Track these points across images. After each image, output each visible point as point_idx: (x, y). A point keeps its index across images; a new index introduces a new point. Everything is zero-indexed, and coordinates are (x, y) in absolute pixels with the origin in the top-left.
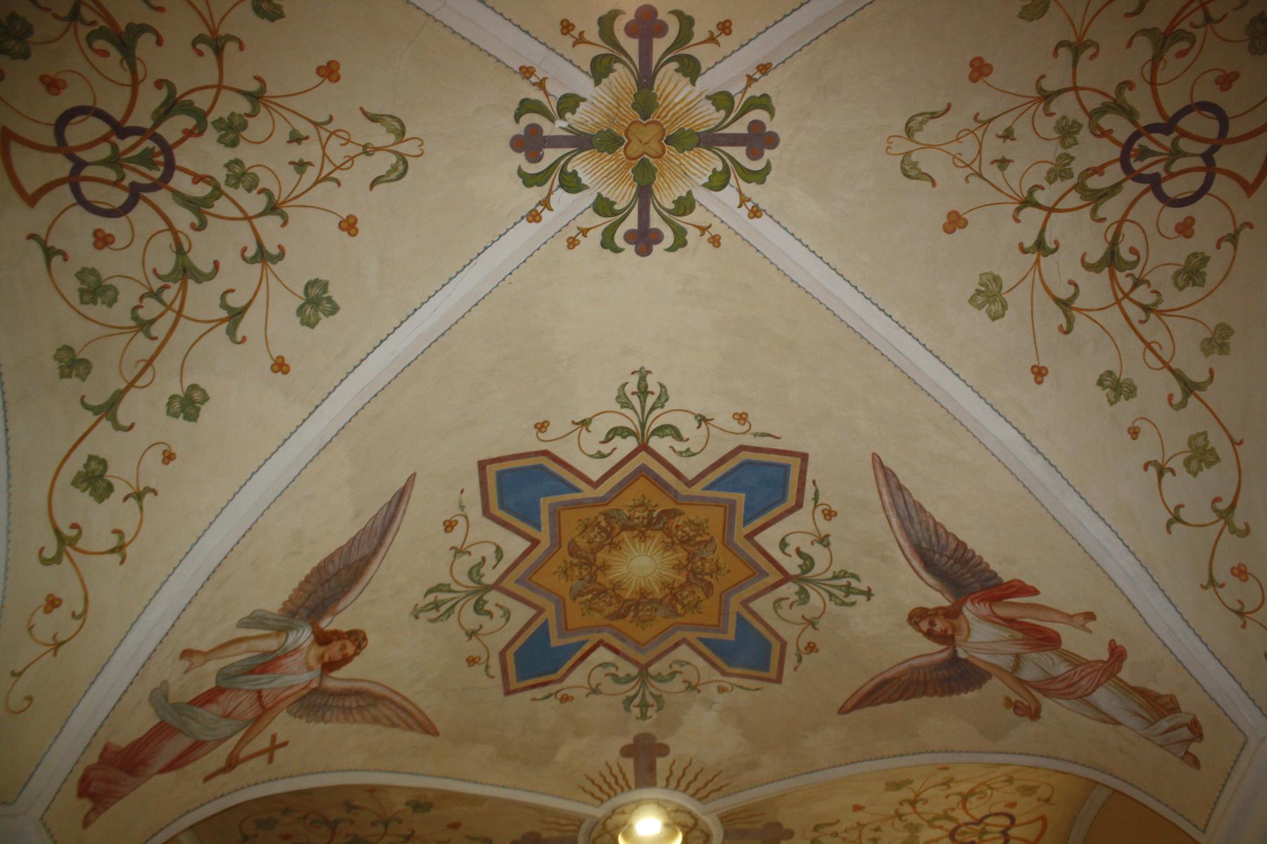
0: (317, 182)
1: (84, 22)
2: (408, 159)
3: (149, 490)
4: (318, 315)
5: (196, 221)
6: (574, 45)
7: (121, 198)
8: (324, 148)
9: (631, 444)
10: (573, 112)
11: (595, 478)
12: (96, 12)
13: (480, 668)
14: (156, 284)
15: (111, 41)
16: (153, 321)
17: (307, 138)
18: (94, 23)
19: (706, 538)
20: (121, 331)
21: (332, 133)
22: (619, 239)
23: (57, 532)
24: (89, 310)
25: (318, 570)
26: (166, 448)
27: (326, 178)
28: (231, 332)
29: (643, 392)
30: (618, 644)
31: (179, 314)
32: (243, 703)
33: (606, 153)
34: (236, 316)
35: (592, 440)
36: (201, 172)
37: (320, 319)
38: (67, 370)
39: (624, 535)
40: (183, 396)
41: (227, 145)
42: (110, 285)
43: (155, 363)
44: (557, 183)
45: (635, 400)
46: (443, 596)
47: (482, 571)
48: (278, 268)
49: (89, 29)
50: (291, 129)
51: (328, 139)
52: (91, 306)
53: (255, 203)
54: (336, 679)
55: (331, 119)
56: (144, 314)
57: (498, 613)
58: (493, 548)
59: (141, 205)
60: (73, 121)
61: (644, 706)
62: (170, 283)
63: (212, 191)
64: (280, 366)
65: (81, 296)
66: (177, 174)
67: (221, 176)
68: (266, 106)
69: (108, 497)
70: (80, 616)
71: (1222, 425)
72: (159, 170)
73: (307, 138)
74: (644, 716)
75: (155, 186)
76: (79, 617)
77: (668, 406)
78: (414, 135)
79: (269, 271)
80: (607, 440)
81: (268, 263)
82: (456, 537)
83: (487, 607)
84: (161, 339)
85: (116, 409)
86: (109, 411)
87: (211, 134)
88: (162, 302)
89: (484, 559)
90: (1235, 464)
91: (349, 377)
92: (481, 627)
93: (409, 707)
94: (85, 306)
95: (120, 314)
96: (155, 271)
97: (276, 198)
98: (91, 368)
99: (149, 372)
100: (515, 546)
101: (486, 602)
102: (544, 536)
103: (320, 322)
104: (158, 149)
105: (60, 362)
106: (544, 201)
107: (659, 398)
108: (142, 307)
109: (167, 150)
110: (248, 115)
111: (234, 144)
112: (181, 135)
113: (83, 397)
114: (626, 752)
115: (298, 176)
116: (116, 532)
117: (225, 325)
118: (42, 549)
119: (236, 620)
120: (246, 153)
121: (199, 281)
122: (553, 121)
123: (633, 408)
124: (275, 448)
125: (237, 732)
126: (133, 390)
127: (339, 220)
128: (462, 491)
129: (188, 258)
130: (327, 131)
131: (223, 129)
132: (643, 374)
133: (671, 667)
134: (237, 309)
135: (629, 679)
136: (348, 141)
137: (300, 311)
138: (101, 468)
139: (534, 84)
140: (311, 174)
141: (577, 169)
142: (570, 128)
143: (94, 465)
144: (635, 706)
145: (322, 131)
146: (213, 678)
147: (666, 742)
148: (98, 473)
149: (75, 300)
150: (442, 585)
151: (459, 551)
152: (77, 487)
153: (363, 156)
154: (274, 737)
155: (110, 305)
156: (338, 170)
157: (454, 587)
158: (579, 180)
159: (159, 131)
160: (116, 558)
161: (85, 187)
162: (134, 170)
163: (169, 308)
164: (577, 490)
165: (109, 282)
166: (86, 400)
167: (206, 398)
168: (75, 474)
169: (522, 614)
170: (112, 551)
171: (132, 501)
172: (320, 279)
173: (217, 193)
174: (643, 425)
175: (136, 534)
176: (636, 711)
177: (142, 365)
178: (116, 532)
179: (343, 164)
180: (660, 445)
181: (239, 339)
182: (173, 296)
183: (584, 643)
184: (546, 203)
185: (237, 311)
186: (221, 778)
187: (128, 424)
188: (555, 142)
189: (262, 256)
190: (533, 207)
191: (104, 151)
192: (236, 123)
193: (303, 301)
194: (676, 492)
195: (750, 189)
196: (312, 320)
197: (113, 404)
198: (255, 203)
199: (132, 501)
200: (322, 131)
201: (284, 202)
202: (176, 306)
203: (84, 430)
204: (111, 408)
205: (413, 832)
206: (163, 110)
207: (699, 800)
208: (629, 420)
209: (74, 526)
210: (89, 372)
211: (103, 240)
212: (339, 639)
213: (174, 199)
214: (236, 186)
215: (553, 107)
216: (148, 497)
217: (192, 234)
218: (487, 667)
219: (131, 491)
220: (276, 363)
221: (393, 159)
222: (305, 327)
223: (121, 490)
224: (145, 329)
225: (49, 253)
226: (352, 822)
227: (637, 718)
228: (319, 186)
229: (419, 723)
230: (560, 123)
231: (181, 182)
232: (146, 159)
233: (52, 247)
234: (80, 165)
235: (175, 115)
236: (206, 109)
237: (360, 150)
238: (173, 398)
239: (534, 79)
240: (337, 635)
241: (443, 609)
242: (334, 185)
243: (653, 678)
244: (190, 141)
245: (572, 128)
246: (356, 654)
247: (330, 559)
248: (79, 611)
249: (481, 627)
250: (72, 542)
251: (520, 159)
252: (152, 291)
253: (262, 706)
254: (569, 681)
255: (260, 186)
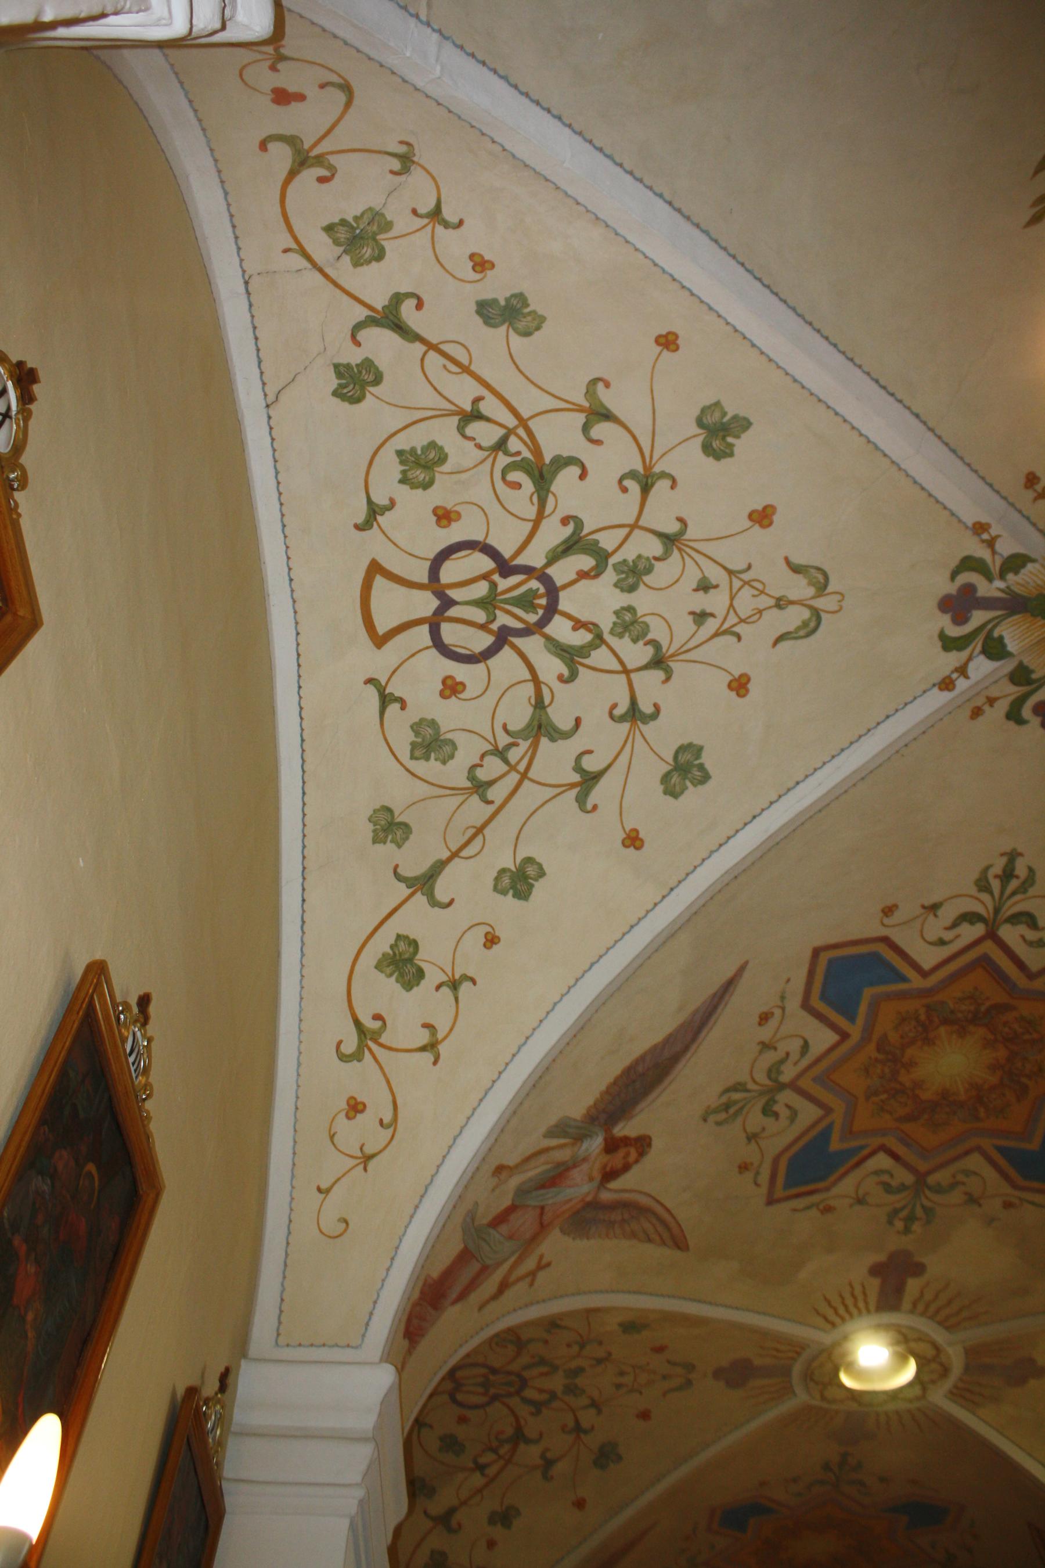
0: (717, 634)
1: (507, 453)
2: (823, 614)
3: (465, 978)
4: (685, 784)
5: (566, 672)
6: (1036, 499)
7: (483, 641)
8: (732, 599)
9: (979, 930)
10: (1016, 573)
11: (926, 966)
12: (525, 443)
13: (749, 1176)
14: (503, 740)
15: (529, 473)
16: (491, 783)
17: (716, 587)
18: (518, 453)
19: (1035, 1036)
20: (448, 792)
21: (746, 583)
22: (1026, 712)
23: (357, 1023)
24: (420, 767)
25: (628, 1070)
26: (490, 929)
27: (726, 632)
28: (581, 801)
29: (1008, 874)
30: (900, 1150)
31: (524, 776)
32: (525, 1222)
33: (1039, 618)
34: (589, 780)
35: (935, 928)
36: (584, 618)
37: (687, 788)
38: (381, 835)
39: (942, 1030)
40: (514, 869)
41: (622, 590)
42: (450, 740)
43: (486, 831)
44: (979, 648)
45: (996, 885)
46: (736, 1096)
47: (783, 1068)
48: (648, 729)
49: (510, 460)
50: (700, 576)
51: (740, 589)
52: (422, 762)
53: (636, 654)
54: (610, 1190)
55: (749, 567)
56: (482, 774)
57: (784, 1113)
58: (801, 1042)
59: (506, 652)
60: (454, 556)
61: (910, 1219)
62: (520, 741)
63: (593, 640)
64: (633, 840)
65: (412, 751)
66: (557, 618)
67: (606, 623)
68: (680, 550)
69: (418, 985)
70: (390, 1125)
71: (546, 392)
72: (537, 614)
73: (716, 587)
74: (907, 1230)
75: (527, 631)
76: (388, 1126)
77: (1031, 892)
78: (836, 589)
79: (637, 732)
80: (954, 925)
81: (639, 722)
82: (765, 1033)
83: (776, 1108)
84: (498, 803)
85: (435, 881)
86: (424, 884)
87: (610, 576)
88: (506, 761)
89: (788, 1054)
90: (712, 537)
91: (713, 856)
92: (764, 1129)
93: (673, 1224)
94: (414, 762)
95: (455, 772)
96: (505, 727)
97: (664, 650)
98: (411, 832)
99: (478, 841)
100: (822, 1038)
101: (775, 1102)
102: (855, 1031)
103: (686, 793)
104: (542, 590)
105: (374, 825)
106: (961, 667)
107: (1024, 883)
108: (481, 766)
109: (553, 591)
110: (656, 559)
111: (632, 589)
112: (574, 576)
113: (397, 866)
114: (876, 1270)
115: (695, 628)
116: (426, 1026)
117: (574, 792)
118: (340, 1043)
119: (543, 1130)
120: (642, 600)
121: (553, 740)
122: (990, 579)
123: (991, 894)
124: (619, 936)
125: (513, 1253)
126: (457, 860)
127: (730, 678)
128: (788, 980)
129: (547, 713)
130: (741, 580)
131: (623, 572)
132: (1013, 856)
133: (954, 1176)
134: (592, 773)
135: (903, 1188)
136: (762, 592)
137: (665, 778)
138: (411, 950)
139: (983, 541)
140: (711, 626)
141: (1004, 634)
142: (1008, 590)
143: (402, 946)
144: (900, 1219)
145: (734, 580)
146: (510, 1196)
147: (924, 1260)
148: (406, 956)
149: (404, 754)
150: (739, 1084)
151: (766, 1046)
152: (382, 972)
153: (775, 610)
154: (541, 1257)
155: (444, 762)
156: (743, 624)
157: (751, 1086)
158: (1003, 646)
159: (549, 571)
160: (428, 1057)
161: (447, 629)
162: (508, 612)
163: (513, 768)
164: (904, 979)
165: (449, 736)
166: (399, 870)
167: (541, 873)
168: (380, 956)
169: (809, 1113)
170: (423, 1049)
171: (445, 990)
172: (695, 742)
173: (598, 642)
174: (997, 911)
175: (451, 1030)
176: (899, 1225)
177: (472, 831)
178: (426, 1026)
179: (750, 617)
180: (1009, 934)
181: (589, 807)
182: (520, 755)
183: (862, 1148)
184: (962, 670)
185: (592, 775)
186: (493, 1306)
187: (447, 900)
188: (987, 604)
189: (634, 715)
190: (947, 673)
191: (481, 589)
192: (641, 566)
193: (670, 768)
194: (1015, 985)
195: (982, 553)
196: (678, 788)
197: (432, 876)
198: (636, 654)
199: (445, 990)
200: (734, 580)
201: (673, 655)
202: (522, 767)
203: (394, 905)
204: (428, 880)
205: (610, 1354)
206: (560, 549)
207: (947, 1328)
208: (984, 904)
209: (377, 1017)
210: (407, 838)
211: (451, 688)
212: (626, 1145)
213: (545, 646)
214: (621, 636)
215: (995, 568)
216: (465, 988)
217: (557, 686)
218: (757, 1173)
219: (445, 979)
220: (628, 837)
221: (806, 614)
222: (668, 797)
223: (433, 976)
224: (481, 790)
225: (385, 699)
226: (546, 1342)
227: (898, 1232)
228: (717, 640)
229: (673, 1237)
230: (999, 584)
231: (529, 1393)
232: (526, 602)
233: (391, 694)
234: (447, 603)
235: (574, 554)
236: (610, 550)
237: (772, 602)
238: (503, 871)
239: (985, 536)
240: (626, 1141)
241: (732, 1111)
242: (735, 639)
243: (929, 1188)
244: (584, 582)
245: (1010, 590)
246: (637, 1161)
247: (642, 1058)
248: (387, 1119)
249: (764, 1129)
250: (375, 1039)
251: (945, 621)
252: (497, 749)
253: (541, 1224)
254: (835, 1191)
255: (650, 637)
